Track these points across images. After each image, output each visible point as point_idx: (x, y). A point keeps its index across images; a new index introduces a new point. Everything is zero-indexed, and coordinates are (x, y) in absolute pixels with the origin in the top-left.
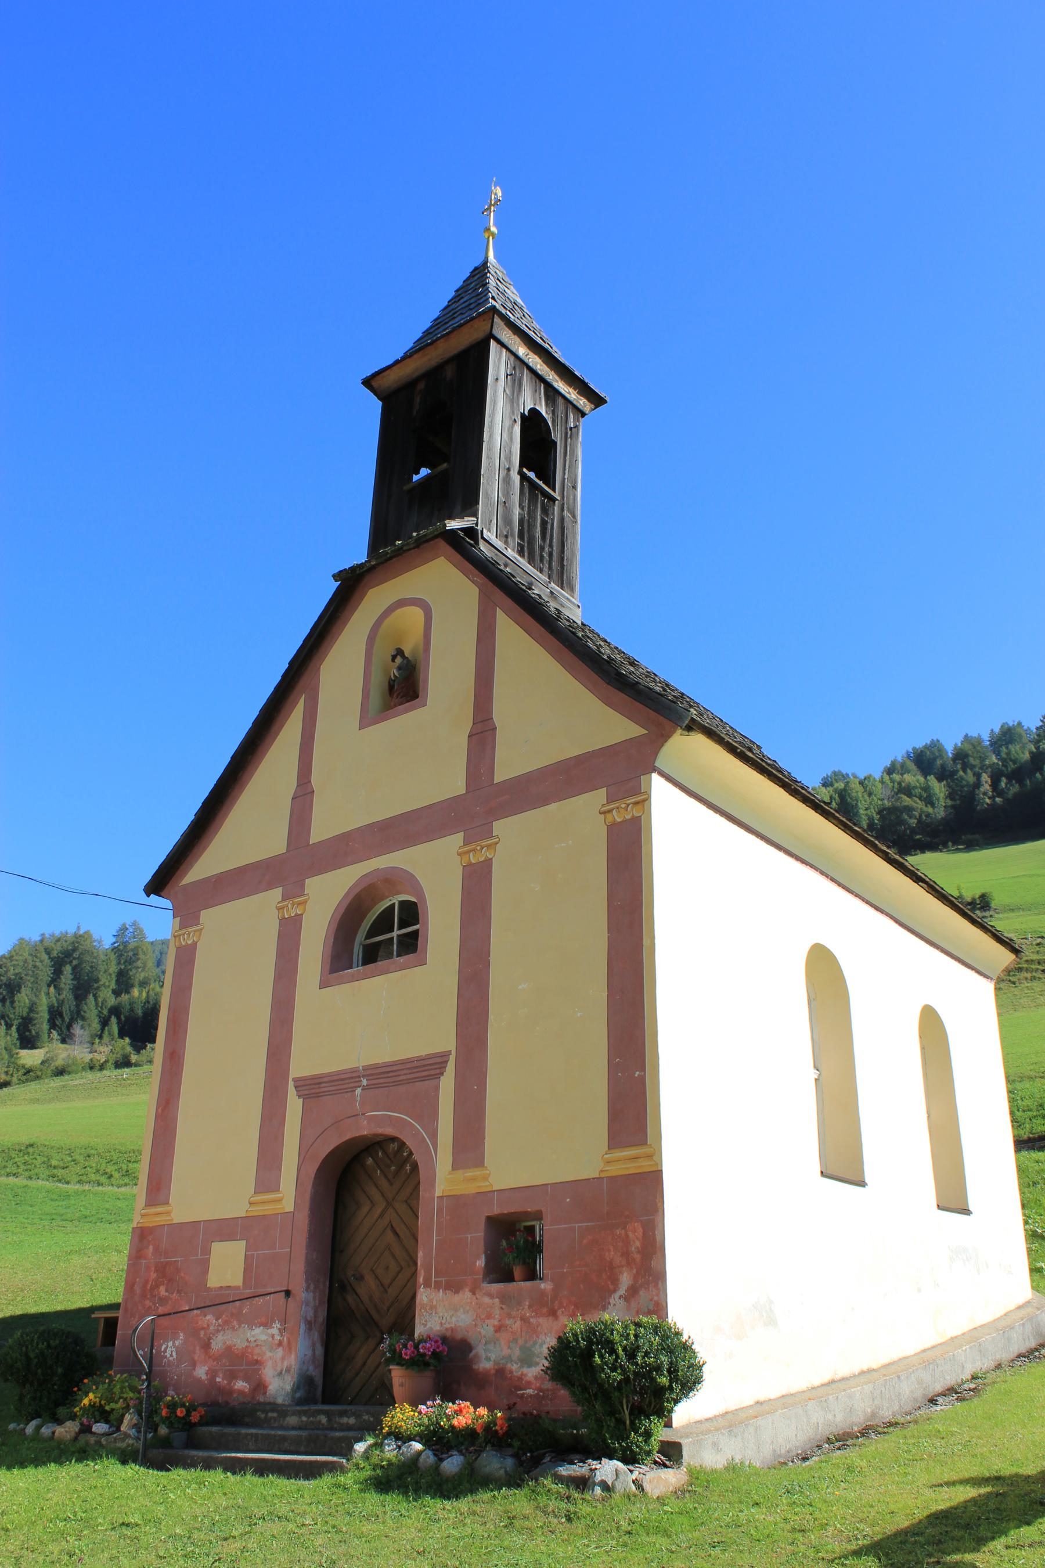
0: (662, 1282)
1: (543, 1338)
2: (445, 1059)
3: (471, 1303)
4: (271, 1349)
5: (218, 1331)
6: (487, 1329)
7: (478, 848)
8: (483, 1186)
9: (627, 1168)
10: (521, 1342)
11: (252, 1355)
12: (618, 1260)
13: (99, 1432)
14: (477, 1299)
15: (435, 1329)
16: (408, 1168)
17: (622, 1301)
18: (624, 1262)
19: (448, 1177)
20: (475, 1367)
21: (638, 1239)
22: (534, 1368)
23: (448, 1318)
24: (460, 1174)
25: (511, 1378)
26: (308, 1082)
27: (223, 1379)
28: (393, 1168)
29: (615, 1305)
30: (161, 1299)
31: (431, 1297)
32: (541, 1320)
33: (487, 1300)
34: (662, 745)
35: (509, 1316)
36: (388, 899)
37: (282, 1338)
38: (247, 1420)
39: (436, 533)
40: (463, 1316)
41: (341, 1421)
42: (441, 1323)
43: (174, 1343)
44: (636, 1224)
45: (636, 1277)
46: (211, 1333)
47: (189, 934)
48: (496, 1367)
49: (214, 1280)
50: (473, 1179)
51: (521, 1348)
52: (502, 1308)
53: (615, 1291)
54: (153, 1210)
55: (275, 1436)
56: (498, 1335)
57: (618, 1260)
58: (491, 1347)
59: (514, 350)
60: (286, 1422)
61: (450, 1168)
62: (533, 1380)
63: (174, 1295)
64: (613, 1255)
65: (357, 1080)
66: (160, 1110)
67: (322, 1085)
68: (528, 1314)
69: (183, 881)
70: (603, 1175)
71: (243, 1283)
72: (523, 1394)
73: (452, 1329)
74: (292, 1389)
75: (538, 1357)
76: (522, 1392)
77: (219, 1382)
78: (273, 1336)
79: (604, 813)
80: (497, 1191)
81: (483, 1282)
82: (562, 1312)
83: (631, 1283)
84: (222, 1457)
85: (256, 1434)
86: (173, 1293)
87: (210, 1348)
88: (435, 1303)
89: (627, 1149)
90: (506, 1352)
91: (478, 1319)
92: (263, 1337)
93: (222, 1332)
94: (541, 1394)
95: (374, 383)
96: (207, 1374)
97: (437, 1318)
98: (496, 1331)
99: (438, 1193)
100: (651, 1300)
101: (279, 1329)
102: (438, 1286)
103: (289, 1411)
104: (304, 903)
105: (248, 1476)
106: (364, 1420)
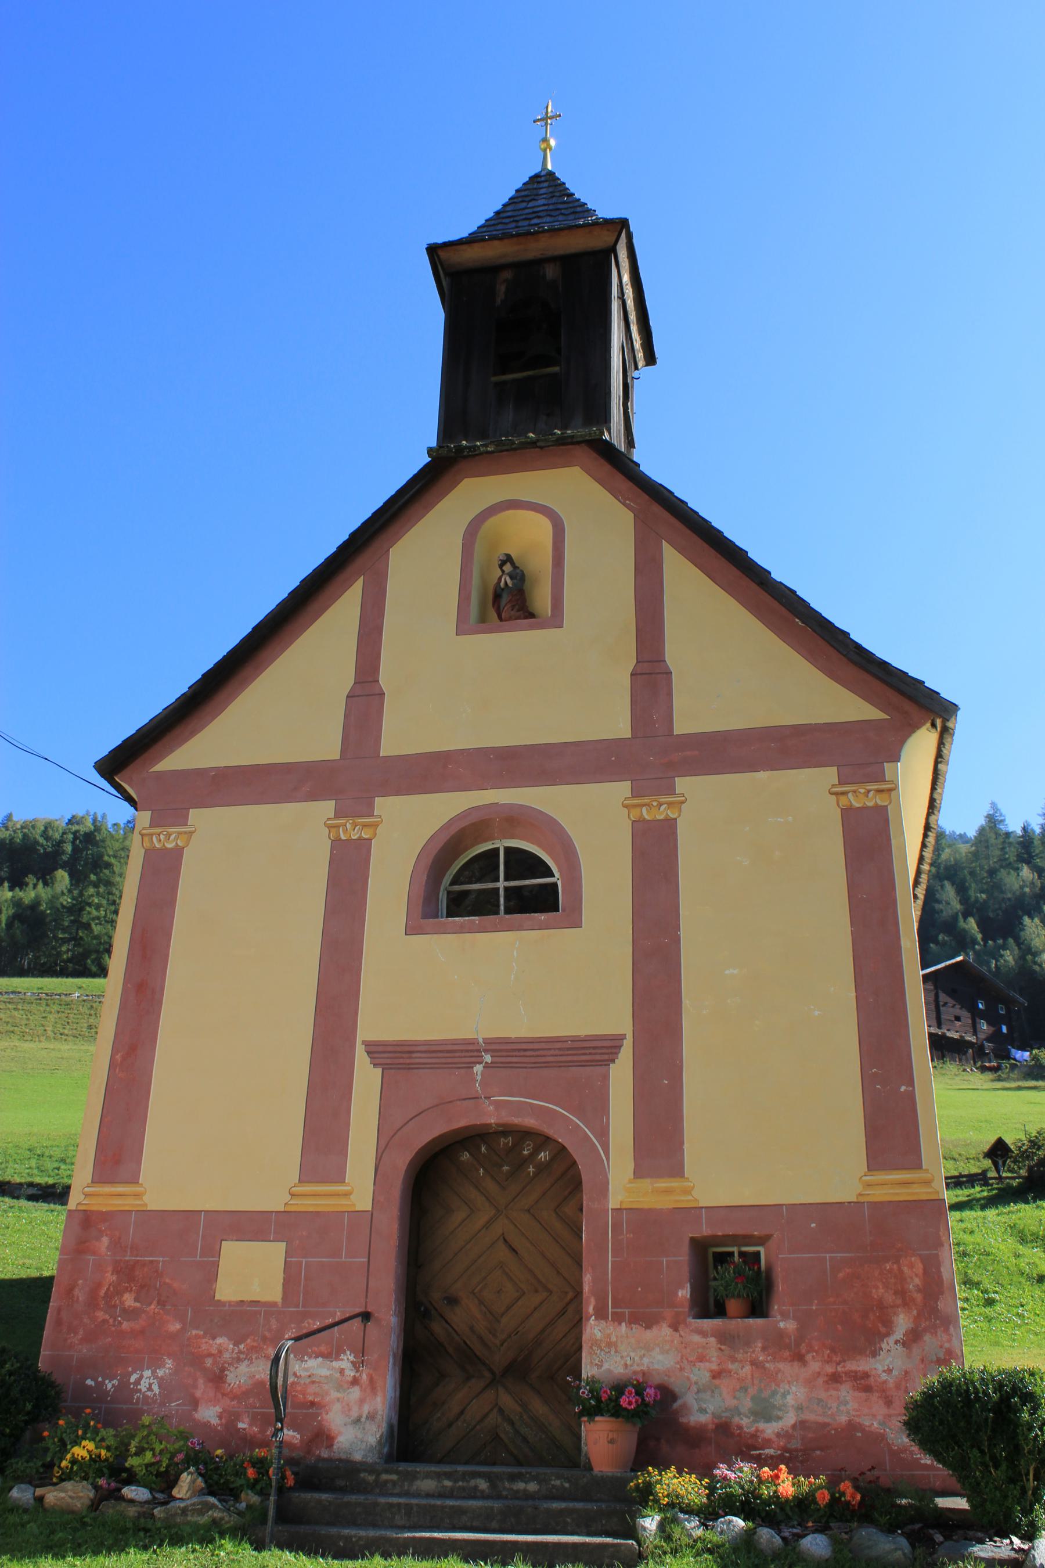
0: (955, 1328)
1: (787, 1387)
2: (616, 1043)
3: (672, 1341)
4: (339, 1387)
5: (239, 1360)
6: (700, 1374)
7: (655, 804)
8: (684, 1201)
9: (897, 1194)
10: (752, 1391)
11: (304, 1395)
12: (889, 1298)
13: (140, 1500)
14: (681, 1336)
15: (616, 1371)
16: (531, 1169)
17: (899, 1347)
18: (899, 1301)
19: (628, 1186)
20: (683, 1420)
21: (917, 1275)
22: (774, 1424)
23: (636, 1359)
24: (646, 1184)
25: (739, 1435)
26: (390, 1049)
27: (251, 1425)
28: (506, 1168)
29: (888, 1351)
30: (125, 1311)
31: (608, 1331)
32: (781, 1366)
33: (696, 1338)
34: (909, 735)
35: (734, 1360)
36: (491, 842)
37: (357, 1375)
38: (341, 1483)
39: (587, 438)
40: (660, 1357)
41: (515, 1488)
42: (626, 1365)
43: (154, 1373)
44: (913, 1259)
45: (917, 1319)
46: (225, 1362)
47: (169, 835)
48: (716, 1421)
49: (226, 1291)
50: (668, 1191)
51: (753, 1399)
52: (720, 1349)
53: (888, 1334)
54: (107, 1189)
55: (443, 1507)
56: (717, 1382)
57: (889, 1298)
58: (707, 1396)
59: (622, 274)
60: (415, 1487)
61: (632, 1176)
62: (773, 1437)
63: (153, 1307)
64: (879, 1292)
65: (475, 1054)
66: (118, 1057)
67: (414, 1055)
68: (761, 1358)
69: (155, 767)
70: (861, 1199)
71: (282, 1299)
72: (760, 1454)
73: (644, 1374)
74: (379, 1442)
75: (780, 1410)
76: (758, 1452)
77: (244, 1429)
78: (342, 1371)
79: (836, 794)
80: (706, 1208)
81: (689, 1316)
82: (813, 1356)
83: (911, 1325)
84: (405, 1538)
85: (407, 1505)
86: (150, 1304)
87: (225, 1382)
88: (614, 1339)
89: (895, 1172)
90: (731, 1402)
91: (685, 1362)
92: (324, 1372)
93: (246, 1362)
94: (787, 1455)
95: (443, 254)
96: (220, 1417)
97: (619, 1359)
98: (714, 1377)
99: (613, 1203)
100: (941, 1347)
101: (352, 1362)
102: (618, 1319)
103: (418, 1472)
104: (375, 826)
105: (132, 1556)
106: (554, 1486)
